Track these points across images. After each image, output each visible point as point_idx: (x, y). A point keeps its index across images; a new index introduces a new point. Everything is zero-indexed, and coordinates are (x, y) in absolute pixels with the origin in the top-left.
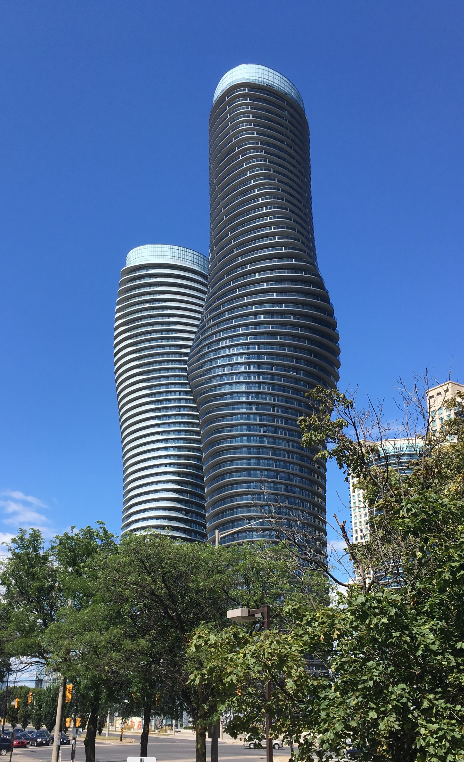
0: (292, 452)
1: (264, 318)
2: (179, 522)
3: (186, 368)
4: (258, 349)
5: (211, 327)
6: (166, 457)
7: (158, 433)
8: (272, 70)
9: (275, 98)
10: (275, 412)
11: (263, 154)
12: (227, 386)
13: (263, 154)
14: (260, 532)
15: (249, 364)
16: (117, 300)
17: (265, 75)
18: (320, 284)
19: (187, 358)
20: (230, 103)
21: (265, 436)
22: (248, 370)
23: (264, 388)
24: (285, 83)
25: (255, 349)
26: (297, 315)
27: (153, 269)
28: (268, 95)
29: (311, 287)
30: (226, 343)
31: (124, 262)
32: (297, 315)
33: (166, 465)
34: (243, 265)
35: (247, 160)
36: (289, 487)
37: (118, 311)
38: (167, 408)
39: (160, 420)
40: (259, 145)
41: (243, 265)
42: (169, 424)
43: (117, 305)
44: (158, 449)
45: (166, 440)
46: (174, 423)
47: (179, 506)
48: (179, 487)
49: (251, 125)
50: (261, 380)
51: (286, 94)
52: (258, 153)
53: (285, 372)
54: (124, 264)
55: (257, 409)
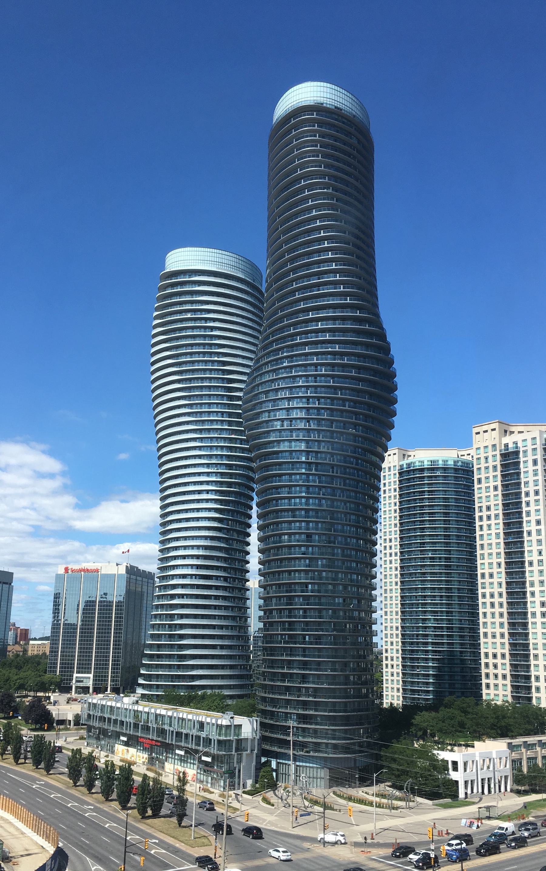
0: (348, 513)
1: (326, 371)
2: (179, 391)
3: (242, 422)
4: (319, 404)
5: (268, 372)
6: (208, 483)
7: (200, 457)
8: (339, 88)
9: (343, 123)
10: (329, 449)
11: (330, 191)
12: (286, 442)
13: (330, 191)
14: (303, 549)
15: (308, 420)
16: (156, 305)
17: (333, 96)
18: (382, 336)
19: (240, 403)
20: (296, 127)
21: (324, 498)
22: (307, 427)
23: (324, 447)
24: (354, 103)
25: (314, 403)
26: (359, 368)
27: (203, 296)
28: (336, 120)
29: (374, 341)
30: (285, 394)
31: (163, 265)
32: (359, 368)
33: (208, 492)
34: (306, 311)
35: (310, 187)
36: (335, 515)
37: (157, 317)
38: (209, 430)
39: (202, 443)
40: (323, 168)
41: (306, 311)
42: (211, 447)
43: (156, 310)
44: (199, 474)
45: (208, 465)
46: (217, 447)
47: (217, 515)
48: (221, 516)
49: (325, 178)
50: (321, 439)
51: (354, 116)
52: (325, 190)
53: (344, 429)
54: (163, 267)
55: (316, 470)
